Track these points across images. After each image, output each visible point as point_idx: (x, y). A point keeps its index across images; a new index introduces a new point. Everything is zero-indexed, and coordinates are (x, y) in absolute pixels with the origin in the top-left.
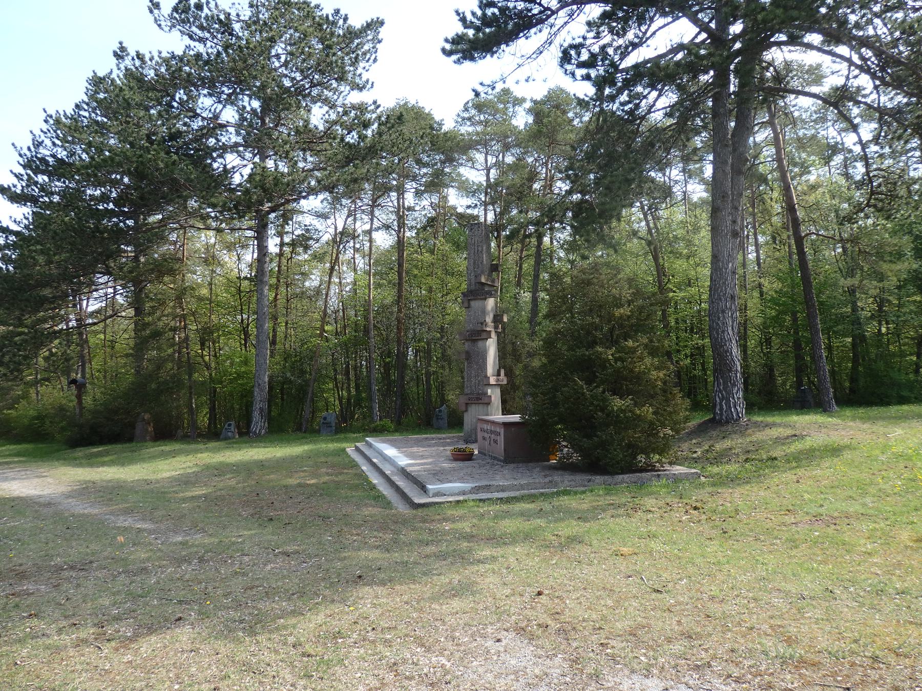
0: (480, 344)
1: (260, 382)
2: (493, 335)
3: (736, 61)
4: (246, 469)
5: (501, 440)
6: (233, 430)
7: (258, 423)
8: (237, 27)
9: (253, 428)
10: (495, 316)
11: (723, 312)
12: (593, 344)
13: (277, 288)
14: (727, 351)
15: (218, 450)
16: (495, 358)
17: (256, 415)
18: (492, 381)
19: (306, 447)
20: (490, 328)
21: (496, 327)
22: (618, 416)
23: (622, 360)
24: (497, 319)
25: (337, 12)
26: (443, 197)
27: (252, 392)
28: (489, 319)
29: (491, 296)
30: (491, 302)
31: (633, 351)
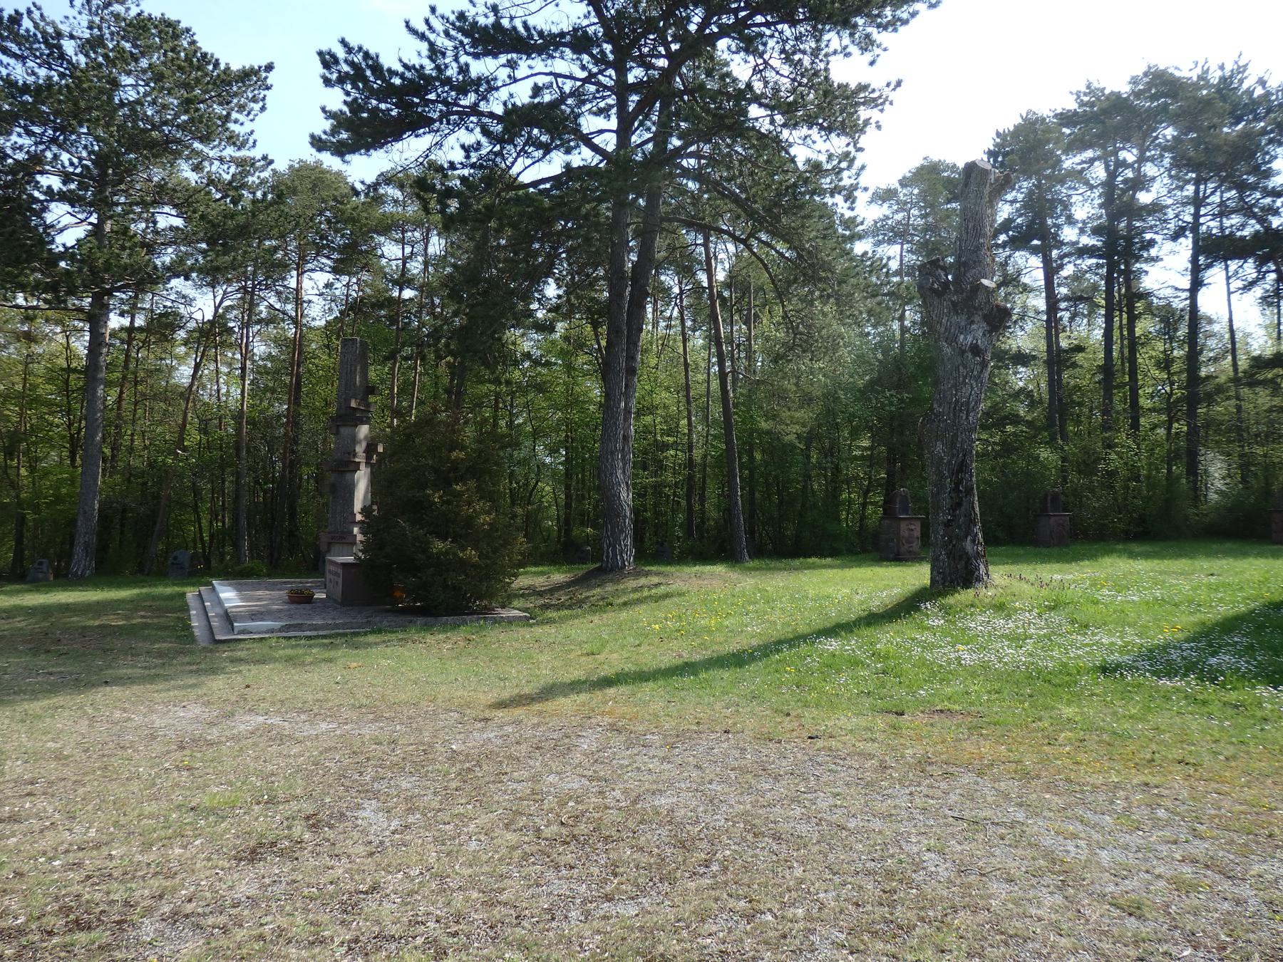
0: (348, 476)
1: (87, 508)
2: (363, 466)
4: (46, 611)
6: (45, 569)
7: (81, 560)
8: (69, 47)
10: (368, 445)
11: (612, 453)
12: (423, 487)
13: (122, 386)
14: (614, 495)
15: (18, 592)
16: (366, 493)
17: (79, 550)
18: (359, 517)
19: (136, 591)
20: (360, 458)
21: (368, 458)
22: (438, 558)
23: (448, 503)
27: (76, 521)
28: (360, 449)
29: (363, 423)
30: (364, 430)
31: (460, 494)
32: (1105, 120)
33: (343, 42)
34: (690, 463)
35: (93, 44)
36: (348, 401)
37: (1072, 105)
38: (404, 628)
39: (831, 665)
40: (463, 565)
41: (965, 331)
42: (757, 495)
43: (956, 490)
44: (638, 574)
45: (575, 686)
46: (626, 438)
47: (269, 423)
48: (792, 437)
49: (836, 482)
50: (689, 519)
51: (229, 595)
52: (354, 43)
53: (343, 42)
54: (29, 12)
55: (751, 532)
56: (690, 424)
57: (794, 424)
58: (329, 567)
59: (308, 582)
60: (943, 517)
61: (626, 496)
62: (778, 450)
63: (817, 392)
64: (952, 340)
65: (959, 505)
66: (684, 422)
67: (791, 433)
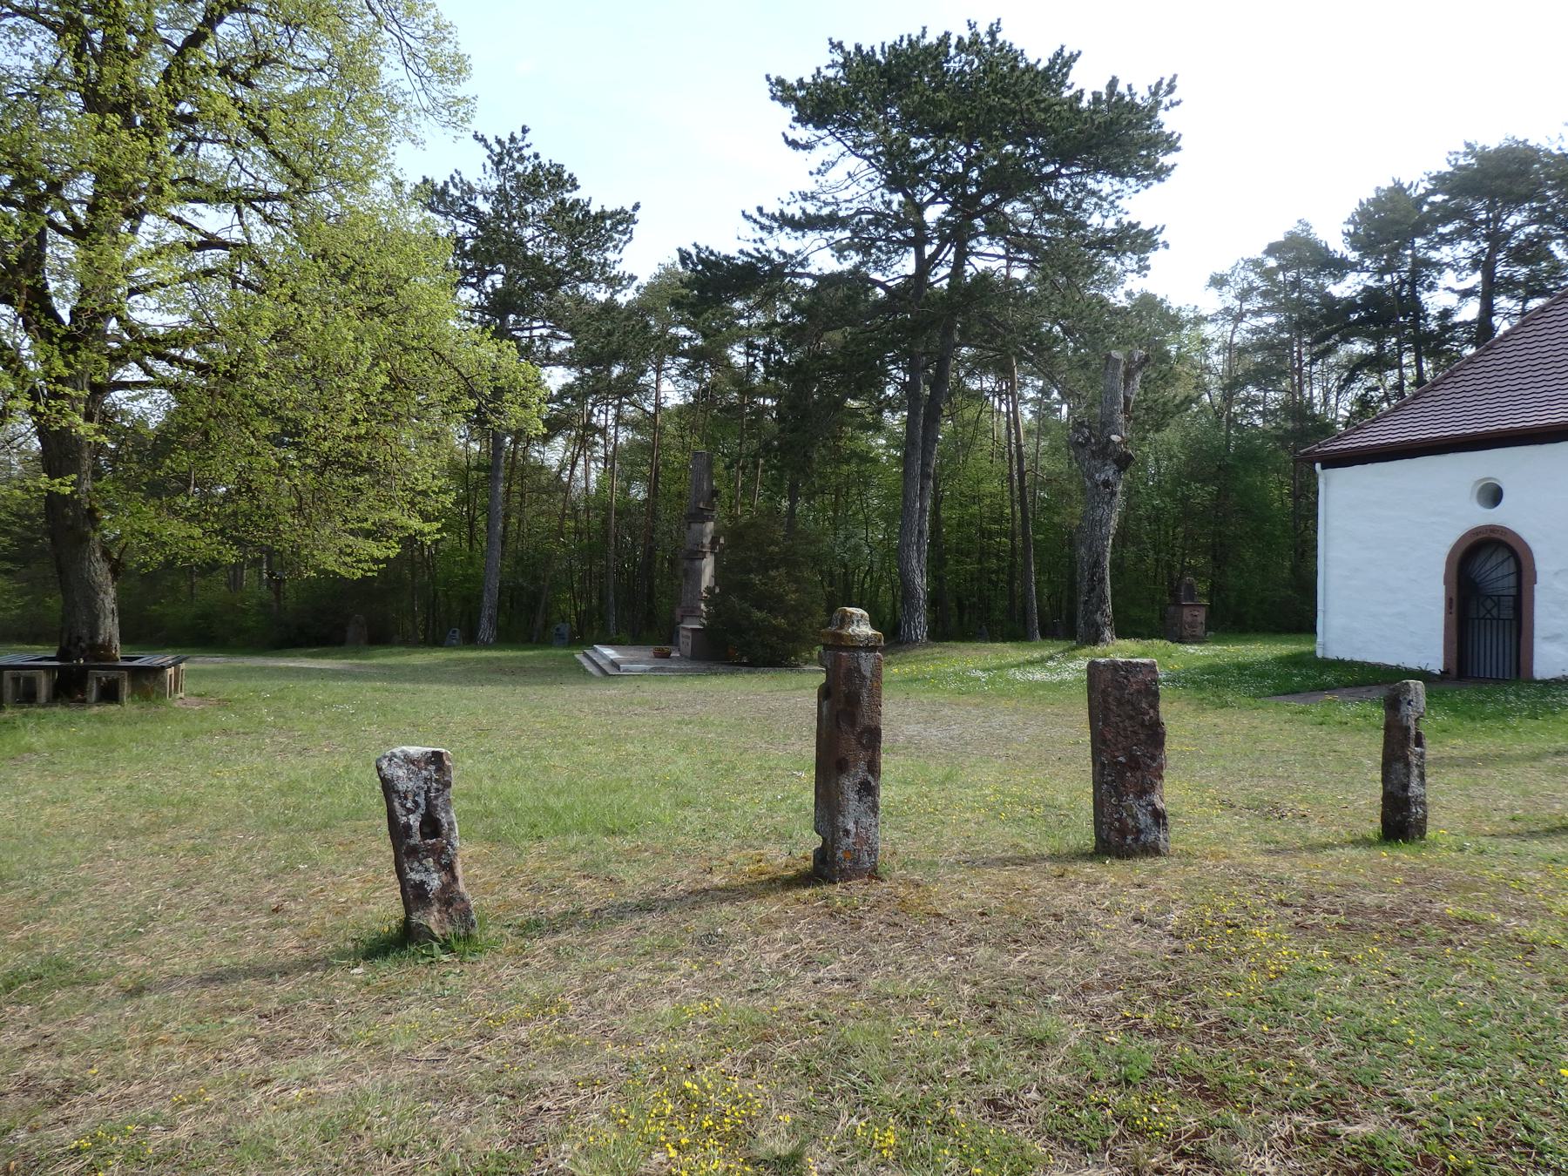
7: (486, 631)
17: (484, 622)
21: (712, 548)
28: (707, 541)
30: (710, 526)
31: (774, 578)
33: (695, 245)
35: (502, 196)
40: (776, 630)
46: (921, 532)
47: (625, 510)
51: (610, 653)
52: (702, 246)
53: (695, 245)
54: (452, 178)
58: (682, 633)
59: (666, 648)
60: (1083, 598)
64: (1091, 477)
65: (1093, 589)
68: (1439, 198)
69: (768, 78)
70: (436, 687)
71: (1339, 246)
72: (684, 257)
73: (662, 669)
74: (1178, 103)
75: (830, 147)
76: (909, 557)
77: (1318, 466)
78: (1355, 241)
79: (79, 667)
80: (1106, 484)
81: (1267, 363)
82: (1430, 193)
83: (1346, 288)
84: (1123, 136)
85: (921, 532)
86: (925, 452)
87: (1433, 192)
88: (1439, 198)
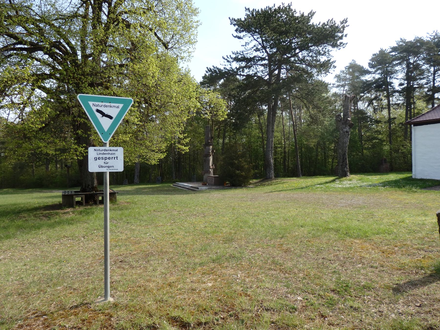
3: (220, 83)
5: (213, 180)
7: (136, 179)
9: (135, 181)
17: (136, 177)
18: (211, 167)
24: (213, 151)
25: (334, 62)
26: (389, 183)
27: (135, 170)
28: (210, 151)
30: (211, 147)
31: (241, 161)
32: (408, 50)
34: (285, 152)
36: (208, 140)
37: (396, 45)
38: (228, 189)
39: (317, 188)
41: (345, 128)
42: (303, 160)
43: (343, 159)
44: (275, 180)
45: (277, 191)
46: (272, 147)
48: (312, 146)
49: (326, 157)
50: (285, 168)
52: (215, 66)
55: (302, 170)
56: (284, 142)
57: (313, 143)
60: (341, 164)
61: (272, 161)
62: (309, 149)
63: (319, 134)
65: (344, 161)
66: (283, 141)
67: (312, 145)
68: (393, 53)
69: (229, 18)
70: (141, 196)
71: (366, 67)
72: (210, 70)
73: (211, 188)
74: (348, 26)
75: (247, 37)
76: (269, 154)
77: (412, 125)
78: (371, 66)
79: (93, 193)
80: (347, 132)
81: (350, 100)
82: (391, 52)
83: (368, 78)
84: (329, 35)
85: (272, 147)
86: (275, 124)
87: (391, 52)
88: (393, 53)
